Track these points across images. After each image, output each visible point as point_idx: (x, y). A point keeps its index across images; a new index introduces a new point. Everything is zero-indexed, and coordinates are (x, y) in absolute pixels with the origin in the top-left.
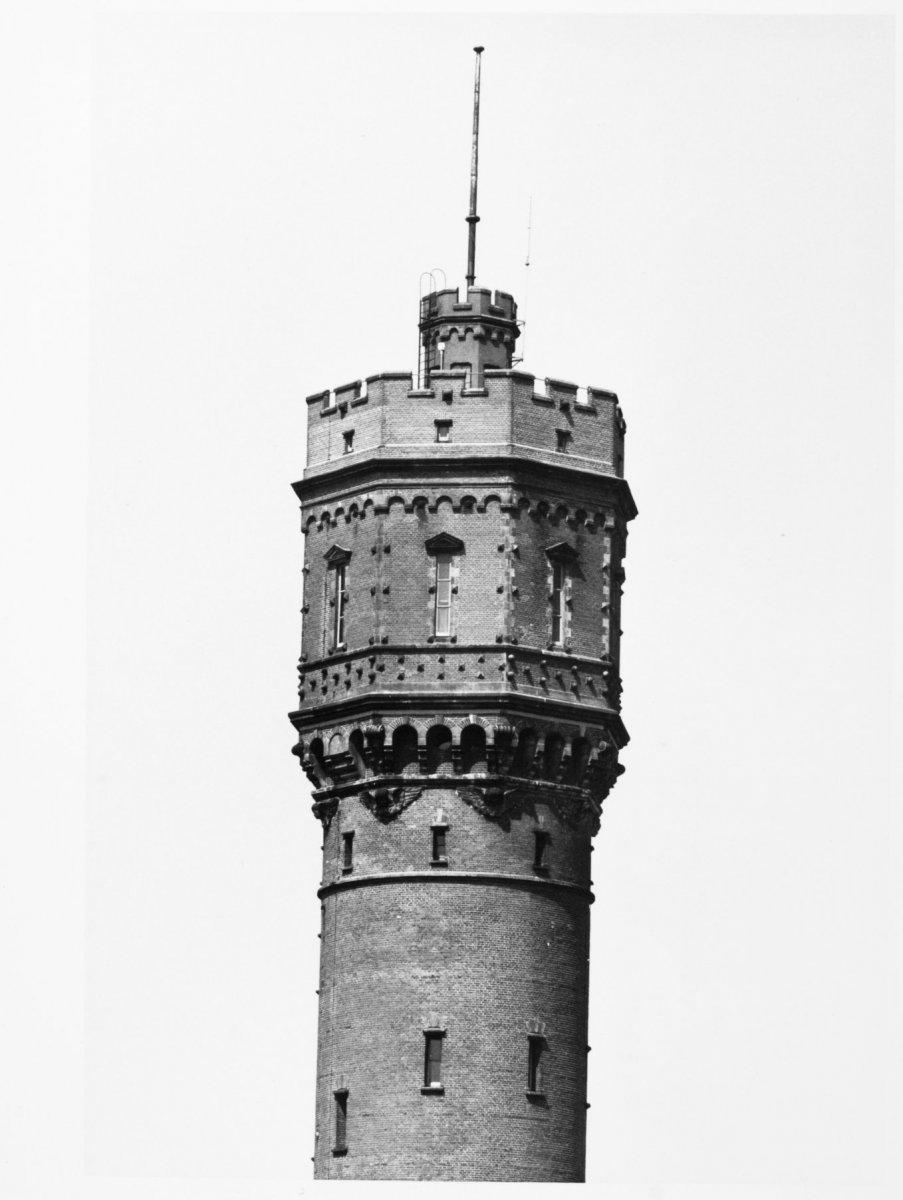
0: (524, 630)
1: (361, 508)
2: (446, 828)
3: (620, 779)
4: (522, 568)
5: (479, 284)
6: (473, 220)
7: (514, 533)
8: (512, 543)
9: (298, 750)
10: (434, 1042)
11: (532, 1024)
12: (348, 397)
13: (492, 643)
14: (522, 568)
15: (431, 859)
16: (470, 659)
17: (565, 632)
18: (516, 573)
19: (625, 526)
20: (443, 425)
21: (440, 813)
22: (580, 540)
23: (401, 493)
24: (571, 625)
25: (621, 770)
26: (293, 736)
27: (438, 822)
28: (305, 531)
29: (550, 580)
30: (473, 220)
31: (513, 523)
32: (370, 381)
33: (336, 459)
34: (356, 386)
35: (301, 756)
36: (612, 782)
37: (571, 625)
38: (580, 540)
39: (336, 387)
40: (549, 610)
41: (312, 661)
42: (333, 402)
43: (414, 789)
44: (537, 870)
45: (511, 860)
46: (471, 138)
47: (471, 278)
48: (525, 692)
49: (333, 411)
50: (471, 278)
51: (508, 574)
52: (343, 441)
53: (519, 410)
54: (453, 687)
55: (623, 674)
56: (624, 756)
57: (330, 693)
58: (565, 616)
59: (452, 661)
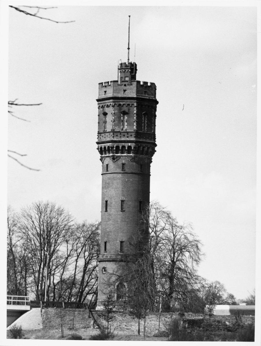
0: (116, 128)
1: (104, 106)
2: (108, 164)
3: (155, 153)
4: (116, 117)
5: (130, 61)
6: (129, 49)
7: (114, 110)
8: (113, 112)
9: (98, 149)
10: (123, 202)
11: (122, 198)
12: (107, 84)
13: (110, 131)
14: (116, 117)
15: (106, 170)
16: (108, 134)
17: (126, 127)
18: (114, 118)
19: (156, 106)
20: (125, 91)
21: (107, 162)
22: (129, 110)
23: (116, 103)
24: (127, 125)
25: (156, 151)
26: (96, 146)
27: (107, 164)
28: (99, 108)
29: (122, 118)
30: (129, 49)
31: (114, 109)
32: (111, 82)
33: (103, 96)
34: (108, 82)
35: (98, 150)
36: (154, 153)
37: (127, 125)
38: (129, 110)
39: (111, 80)
40: (122, 123)
41: (100, 132)
42: (104, 84)
43: (104, 158)
44: (141, 171)
45: (117, 169)
46: (128, 33)
47: (129, 60)
48: (117, 139)
49: (104, 87)
50: (129, 60)
51: (112, 118)
52: (104, 93)
53: (115, 88)
54: (114, 139)
55: (156, 134)
56: (156, 149)
57: (106, 138)
58: (126, 124)
59: (106, 134)
